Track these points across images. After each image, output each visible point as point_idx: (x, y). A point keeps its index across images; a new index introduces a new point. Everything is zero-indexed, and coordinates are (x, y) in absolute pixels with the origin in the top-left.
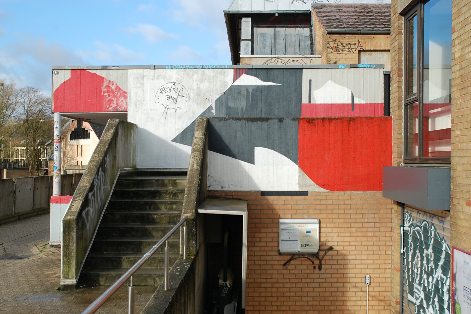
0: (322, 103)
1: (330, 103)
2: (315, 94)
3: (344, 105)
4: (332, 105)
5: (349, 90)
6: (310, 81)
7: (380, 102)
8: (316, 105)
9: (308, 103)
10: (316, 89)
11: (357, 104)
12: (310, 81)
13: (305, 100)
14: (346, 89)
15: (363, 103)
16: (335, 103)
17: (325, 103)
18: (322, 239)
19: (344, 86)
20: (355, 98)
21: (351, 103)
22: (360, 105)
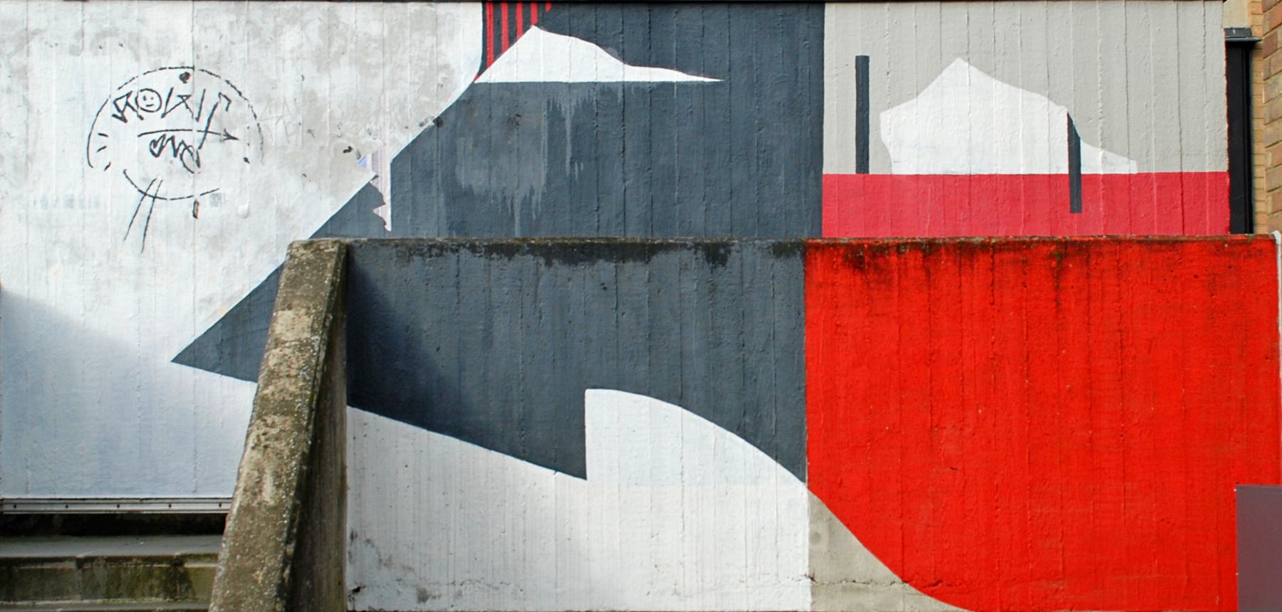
0: (923, 171)
2: (885, 124)
6: (862, 64)
9: (851, 169)
11: (1094, 177)
12: (862, 64)
13: (838, 158)
17: (939, 171)
19: (1027, 87)
20: (1083, 145)
21: (1064, 170)
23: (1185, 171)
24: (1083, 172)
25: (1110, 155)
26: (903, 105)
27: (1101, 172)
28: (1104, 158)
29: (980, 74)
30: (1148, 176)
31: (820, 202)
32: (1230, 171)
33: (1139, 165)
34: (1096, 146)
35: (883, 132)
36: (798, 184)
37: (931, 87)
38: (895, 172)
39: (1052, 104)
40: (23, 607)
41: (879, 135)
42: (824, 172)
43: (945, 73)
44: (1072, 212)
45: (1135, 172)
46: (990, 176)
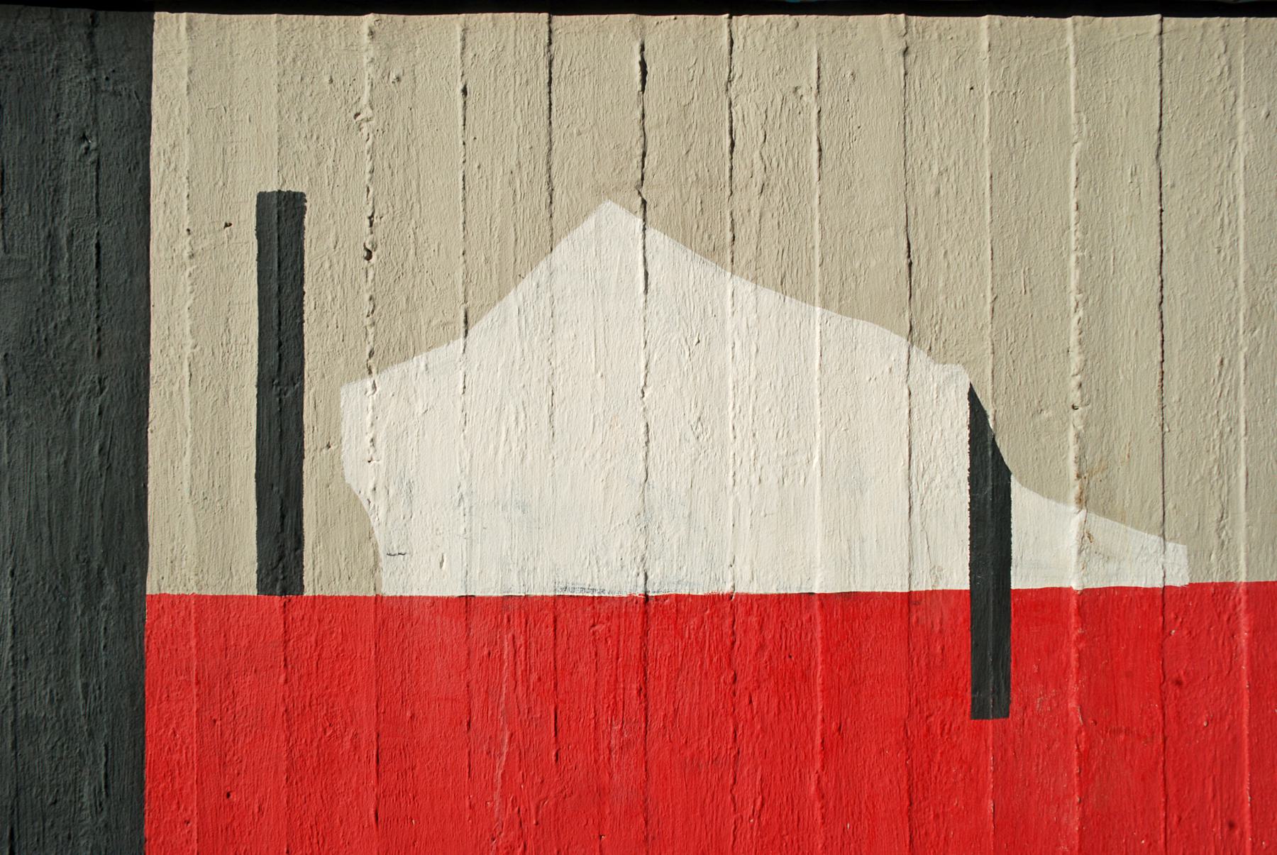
0: (488, 586)
1: (617, 580)
2: (364, 428)
3: (848, 609)
4: (651, 614)
5: (937, 373)
6: (282, 219)
7: (163, 14)
8: (392, 623)
9: (243, 579)
10: (375, 361)
11: (1051, 600)
12: (282, 219)
13: (197, 541)
14: (880, 347)
15: (1148, 578)
16: (700, 585)
17: (541, 585)
18: (639, 222)
19: (841, 299)
20: (1023, 500)
21: (958, 578)
22: (1105, 608)
23: (913, 589)
24: (1016, 583)
25: (1100, 524)
26: (420, 361)
27: (1076, 585)
28: (1086, 536)
29: (685, 256)
30: (1224, 590)
31: (136, 691)
32: (971, 591)
33: (1193, 555)
34: (1060, 498)
35: (353, 450)
36: (62, 628)
37: (512, 300)
38: (388, 590)
39: (920, 357)
40: (995, 425)
41: (335, 466)
42: (152, 588)
43: (563, 247)
44: (979, 712)
45: (1179, 578)
46: (714, 601)
